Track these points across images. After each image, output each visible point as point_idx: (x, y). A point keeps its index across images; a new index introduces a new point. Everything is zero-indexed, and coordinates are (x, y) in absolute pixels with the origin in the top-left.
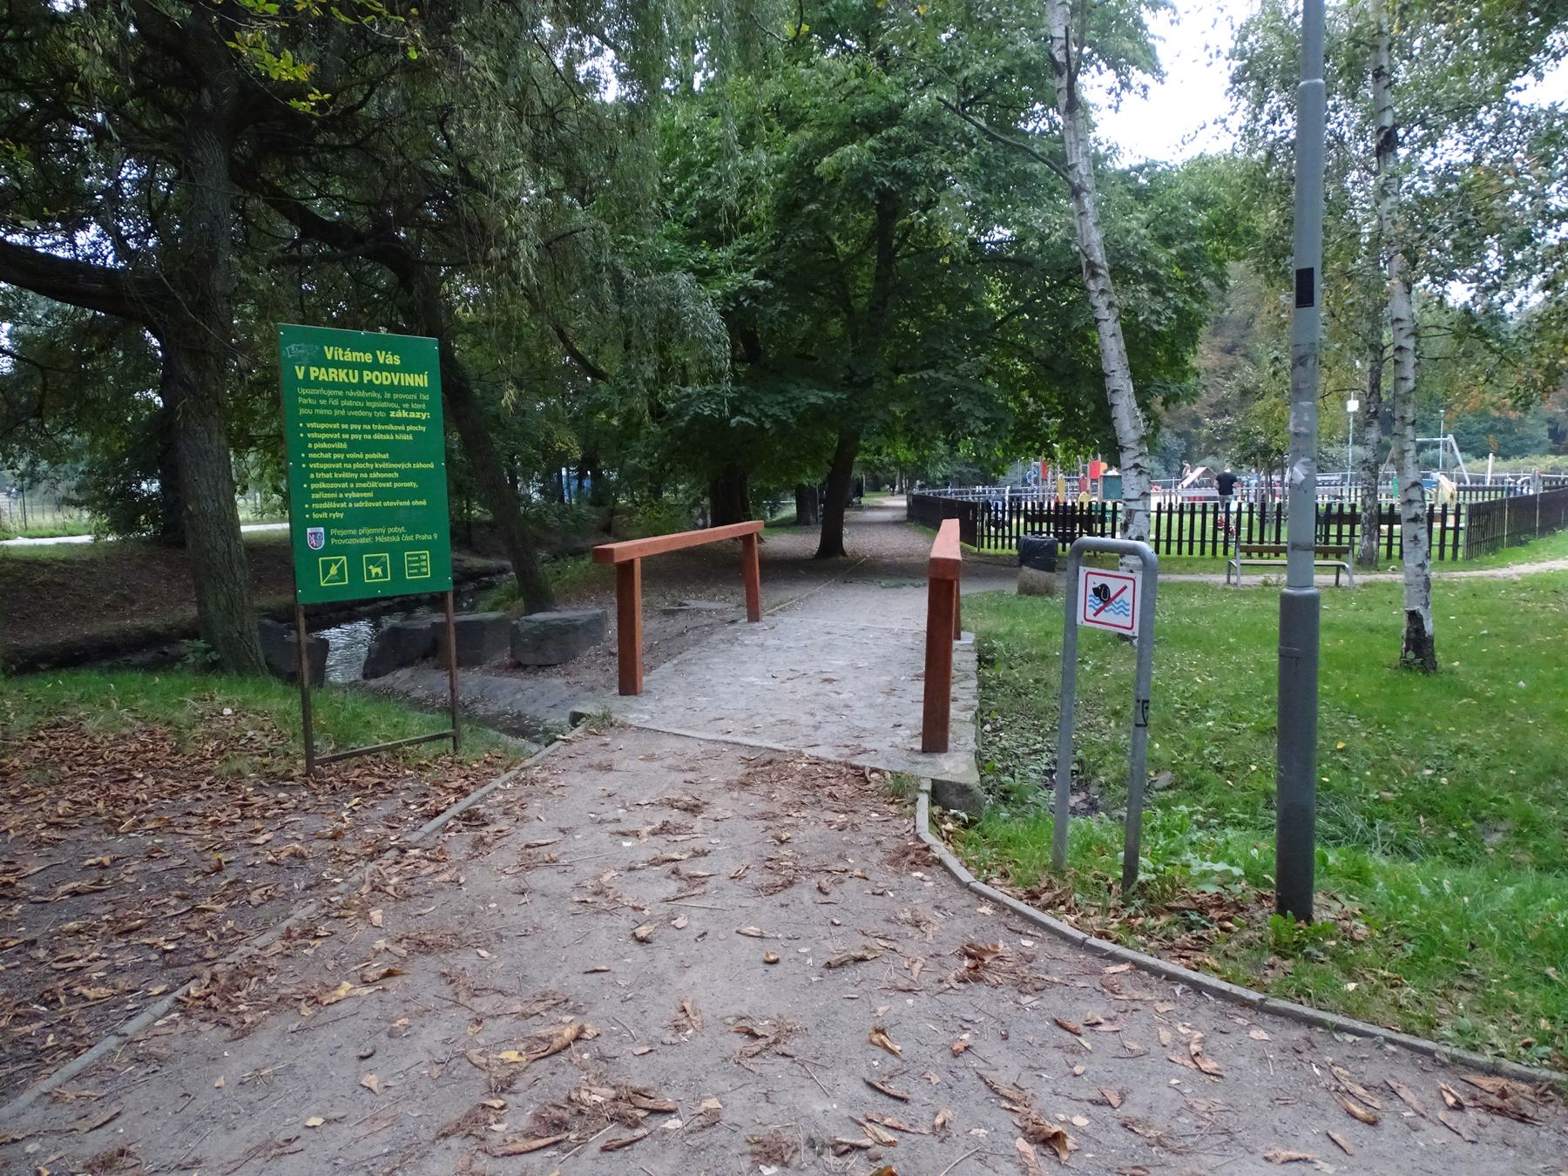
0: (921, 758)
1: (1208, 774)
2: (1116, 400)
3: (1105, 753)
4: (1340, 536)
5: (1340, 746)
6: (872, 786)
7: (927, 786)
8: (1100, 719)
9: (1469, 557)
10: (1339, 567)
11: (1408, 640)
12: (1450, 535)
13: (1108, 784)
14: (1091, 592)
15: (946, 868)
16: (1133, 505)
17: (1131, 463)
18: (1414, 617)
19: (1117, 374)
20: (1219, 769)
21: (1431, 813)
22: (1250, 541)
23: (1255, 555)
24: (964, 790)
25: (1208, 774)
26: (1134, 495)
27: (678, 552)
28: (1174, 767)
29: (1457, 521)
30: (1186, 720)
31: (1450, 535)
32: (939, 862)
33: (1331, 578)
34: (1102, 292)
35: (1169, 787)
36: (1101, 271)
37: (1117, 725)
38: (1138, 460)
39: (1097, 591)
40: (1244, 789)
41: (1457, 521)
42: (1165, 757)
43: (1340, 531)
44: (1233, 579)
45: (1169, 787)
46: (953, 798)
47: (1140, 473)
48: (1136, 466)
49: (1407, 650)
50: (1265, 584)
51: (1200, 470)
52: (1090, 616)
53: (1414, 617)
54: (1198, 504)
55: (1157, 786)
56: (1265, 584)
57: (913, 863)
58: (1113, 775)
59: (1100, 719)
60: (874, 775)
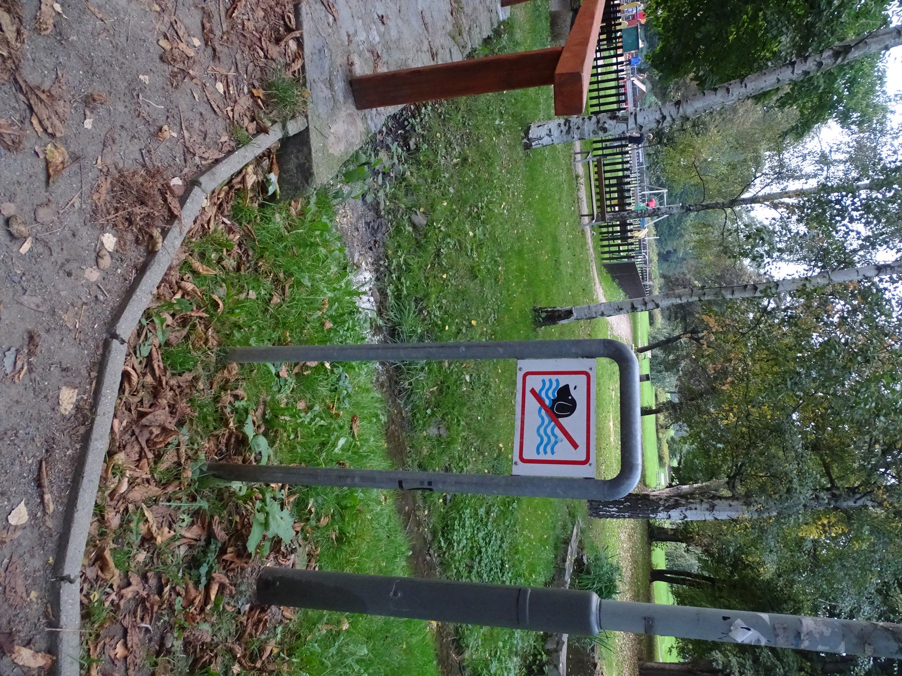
0: (340, 86)
1: (431, 249)
2: (721, 93)
3: (429, 166)
4: (611, 199)
5: (474, 322)
6: (274, 51)
7: (293, 128)
8: (458, 149)
9: (605, 266)
10: (593, 215)
11: (553, 312)
12: (616, 248)
13: (404, 180)
14: (564, 380)
15: (142, 270)
16: (631, 120)
17: (666, 113)
18: (569, 313)
19: (743, 90)
20: (438, 255)
21: (440, 391)
22: (605, 165)
23: (598, 197)
24: (306, 173)
25: (431, 249)
26: (640, 120)
27: (584, 58)
28: (430, 224)
29: (623, 251)
30: (470, 214)
31: (616, 248)
32: (151, 253)
33: (585, 211)
34: (820, 64)
35: (414, 226)
36: (840, 60)
37: (457, 164)
38: (669, 119)
39: (564, 392)
40: (427, 278)
41: (623, 251)
42: (438, 214)
43: (617, 225)
44: (579, 157)
45: (414, 226)
46: (292, 165)
47: (658, 122)
48: (664, 118)
49: (547, 312)
50: (577, 177)
51: (643, 88)
52: (534, 382)
53: (569, 313)
54: (622, 90)
55: (413, 217)
56: (577, 177)
57: (130, 221)
58: (413, 180)
59: (458, 149)
60: (293, 45)
